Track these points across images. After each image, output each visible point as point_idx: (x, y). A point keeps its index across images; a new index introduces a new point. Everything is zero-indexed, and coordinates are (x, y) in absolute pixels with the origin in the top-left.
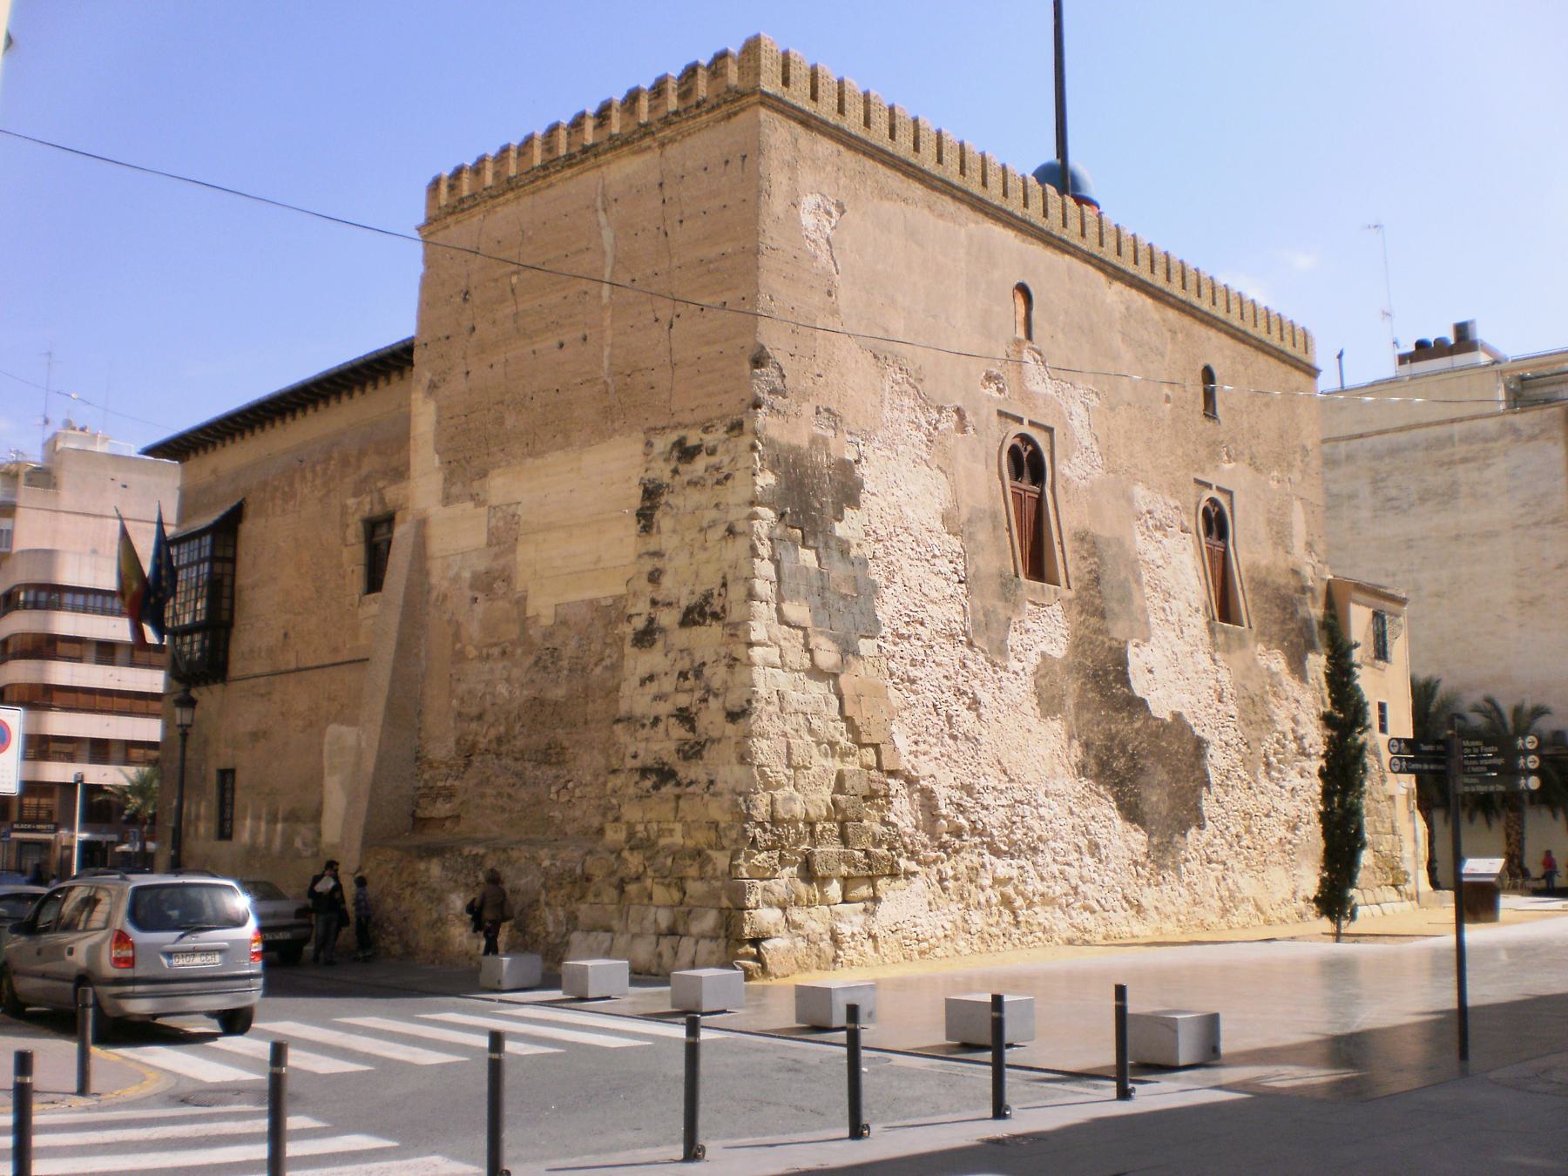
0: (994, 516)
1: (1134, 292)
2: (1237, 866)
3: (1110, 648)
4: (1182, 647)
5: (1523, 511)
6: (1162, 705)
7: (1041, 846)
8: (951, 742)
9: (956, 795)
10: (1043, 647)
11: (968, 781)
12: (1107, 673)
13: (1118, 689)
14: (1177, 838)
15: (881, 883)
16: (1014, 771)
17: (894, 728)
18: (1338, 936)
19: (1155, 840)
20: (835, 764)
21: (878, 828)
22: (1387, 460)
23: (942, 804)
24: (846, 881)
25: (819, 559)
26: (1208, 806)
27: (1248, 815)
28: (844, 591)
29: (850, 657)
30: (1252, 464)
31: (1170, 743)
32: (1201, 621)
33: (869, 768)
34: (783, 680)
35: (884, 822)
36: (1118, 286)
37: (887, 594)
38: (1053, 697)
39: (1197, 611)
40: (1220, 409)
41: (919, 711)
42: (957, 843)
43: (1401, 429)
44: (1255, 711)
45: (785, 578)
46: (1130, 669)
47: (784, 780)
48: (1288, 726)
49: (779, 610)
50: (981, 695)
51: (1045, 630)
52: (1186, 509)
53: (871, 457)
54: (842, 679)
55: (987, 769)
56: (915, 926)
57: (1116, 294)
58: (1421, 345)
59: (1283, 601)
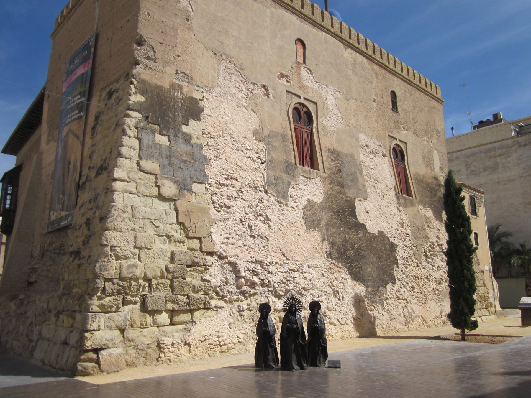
0: (284, 137)
1: (357, 54)
2: (412, 301)
3: (346, 200)
4: (382, 203)
5: (523, 171)
6: (373, 226)
7: (305, 292)
8: (251, 239)
9: (251, 266)
10: (309, 197)
11: (260, 259)
12: (344, 211)
13: (350, 219)
14: (381, 288)
15: (196, 313)
16: (288, 255)
17: (212, 230)
18: (463, 337)
19: (370, 289)
20: (169, 247)
21: (197, 283)
22: (471, 158)
23: (242, 270)
24: (172, 313)
25: (170, 141)
26: (397, 273)
27: (416, 277)
28: (185, 158)
29: (185, 192)
30: (415, 132)
31: (377, 245)
32: (392, 193)
33: (194, 250)
34: (136, 200)
35: (203, 280)
36: (350, 51)
37: (214, 164)
38: (314, 220)
39: (391, 189)
40: (399, 109)
41: (230, 223)
42: (252, 291)
43: (475, 147)
44: (419, 231)
45: (144, 148)
46: (357, 210)
47: (130, 255)
48: (435, 240)
49: (138, 164)
50: (270, 216)
51: (311, 189)
52: (385, 147)
53: (210, 99)
54: (178, 203)
55: (273, 254)
56: (218, 337)
57: (348, 53)
58: (481, 122)
59: (429, 188)
